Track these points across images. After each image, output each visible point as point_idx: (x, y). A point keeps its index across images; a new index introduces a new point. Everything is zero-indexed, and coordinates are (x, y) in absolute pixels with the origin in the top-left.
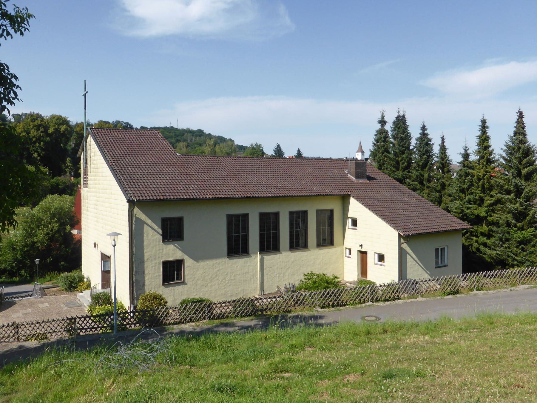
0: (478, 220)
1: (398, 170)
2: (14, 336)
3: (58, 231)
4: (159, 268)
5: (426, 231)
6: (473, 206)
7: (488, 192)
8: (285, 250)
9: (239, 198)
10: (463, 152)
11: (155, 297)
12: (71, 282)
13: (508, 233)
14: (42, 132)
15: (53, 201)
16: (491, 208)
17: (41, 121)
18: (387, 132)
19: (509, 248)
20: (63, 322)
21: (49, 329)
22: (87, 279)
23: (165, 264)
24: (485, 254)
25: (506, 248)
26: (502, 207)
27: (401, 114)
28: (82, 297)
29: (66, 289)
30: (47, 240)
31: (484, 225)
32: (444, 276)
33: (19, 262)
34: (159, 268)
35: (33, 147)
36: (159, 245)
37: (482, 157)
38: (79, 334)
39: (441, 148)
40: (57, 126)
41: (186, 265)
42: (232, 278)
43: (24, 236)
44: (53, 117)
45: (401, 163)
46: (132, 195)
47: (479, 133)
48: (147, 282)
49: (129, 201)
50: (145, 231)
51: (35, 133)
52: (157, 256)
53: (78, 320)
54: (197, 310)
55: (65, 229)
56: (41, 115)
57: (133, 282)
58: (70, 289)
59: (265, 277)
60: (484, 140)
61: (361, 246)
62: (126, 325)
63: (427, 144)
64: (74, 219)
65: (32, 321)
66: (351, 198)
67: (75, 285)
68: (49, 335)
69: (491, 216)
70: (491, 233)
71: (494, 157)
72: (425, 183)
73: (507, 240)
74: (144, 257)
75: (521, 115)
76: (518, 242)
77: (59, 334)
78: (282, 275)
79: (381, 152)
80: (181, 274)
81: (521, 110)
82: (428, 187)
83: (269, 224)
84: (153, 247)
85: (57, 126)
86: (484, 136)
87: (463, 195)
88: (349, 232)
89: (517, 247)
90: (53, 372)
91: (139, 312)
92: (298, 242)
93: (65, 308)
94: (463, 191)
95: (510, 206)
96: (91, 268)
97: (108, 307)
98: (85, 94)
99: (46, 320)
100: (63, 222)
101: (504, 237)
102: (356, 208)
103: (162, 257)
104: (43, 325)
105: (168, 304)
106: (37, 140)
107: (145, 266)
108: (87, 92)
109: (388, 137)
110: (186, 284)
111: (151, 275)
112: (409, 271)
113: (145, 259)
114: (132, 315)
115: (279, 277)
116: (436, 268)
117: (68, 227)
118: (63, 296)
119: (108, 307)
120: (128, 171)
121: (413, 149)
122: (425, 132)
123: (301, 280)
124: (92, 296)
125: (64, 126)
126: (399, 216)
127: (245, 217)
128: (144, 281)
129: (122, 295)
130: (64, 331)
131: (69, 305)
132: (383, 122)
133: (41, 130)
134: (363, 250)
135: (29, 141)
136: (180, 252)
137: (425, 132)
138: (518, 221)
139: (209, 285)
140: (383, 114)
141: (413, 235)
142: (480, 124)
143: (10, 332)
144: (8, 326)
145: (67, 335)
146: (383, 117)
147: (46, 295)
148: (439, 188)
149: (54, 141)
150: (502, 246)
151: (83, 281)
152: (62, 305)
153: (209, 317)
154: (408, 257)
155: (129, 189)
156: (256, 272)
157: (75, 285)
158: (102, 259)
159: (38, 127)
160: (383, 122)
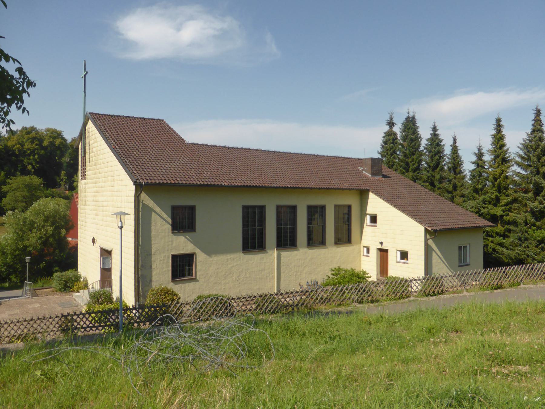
0: (494, 219)
1: (407, 171)
3: (53, 235)
5: (453, 227)
6: (490, 206)
7: (504, 191)
9: (256, 187)
10: (477, 152)
11: (167, 292)
12: (66, 282)
13: (527, 232)
14: (37, 145)
15: (47, 204)
16: (508, 207)
17: (36, 134)
18: (395, 134)
19: (528, 247)
20: (56, 320)
22: (84, 279)
23: (175, 258)
24: (502, 254)
25: (525, 247)
27: (411, 115)
28: (79, 296)
29: (60, 290)
30: (40, 244)
31: (499, 225)
33: (10, 267)
35: (28, 159)
37: (497, 157)
39: (452, 149)
42: (248, 275)
43: (16, 239)
44: (48, 130)
45: (413, 165)
46: (139, 178)
47: (494, 132)
48: (154, 278)
49: (135, 183)
51: (30, 146)
54: (218, 306)
55: (60, 233)
56: (36, 128)
58: (65, 290)
59: (282, 275)
60: (499, 139)
61: (381, 243)
63: (438, 145)
64: (67, 223)
65: (18, 318)
66: (371, 194)
69: (507, 215)
70: (507, 233)
71: (509, 156)
72: (436, 184)
73: (526, 239)
74: (151, 250)
75: (538, 113)
76: (538, 241)
77: (52, 334)
78: (299, 274)
79: (389, 153)
80: (192, 270)
81: (539, 108)
82: (439, 188)
83: (286, 216)
85: (51, 140)
86: (499, 134)
87: (477, 196)
89: (537, 246)
90: (38, 373)
91: (149, 308)
92: (316, 240)
94: (476, 191)
95: (530, 204)
96: (88, 267)
99: (35, 318)
101: (523, 236)
102: (375, 204)
103: (171, 250)
105: (181, 301)
106: (31, 152)
107: (153, 259)
108: (87, 73)
109: (397, 138)
110: (198, 281)
113: (153, 251)
115: (296, 275)
116: (459, 266)
117: (63, 231)
118: (57, 296)
120: (133, 155)
121: (423, 151)
122: (437, 133)
123: (328, 276)
125: (60, 140)
126: (421, 212)
127: (262, 209)
129: (125, 291)
130: (58, 331)
132: (391, 124)
133: (35, 143)
134: (384, 247)
135: (23, 153)
136: (192, 245)
137: (437, 133)
138: (537, 219)
140: (391, 116)
142: (495, 122)
145: (62, 335)
146: (391, 119)
147: (37, 295)
148: (451, 189)
149: (49, 154)
151: (80, 281)
152: (56, 306)
154: (434, 254)
155: (135, 172)
156: (273, 269)
157: (69, 286)
158: (101, 255)
159: (33, 140)
160: (391, 124)
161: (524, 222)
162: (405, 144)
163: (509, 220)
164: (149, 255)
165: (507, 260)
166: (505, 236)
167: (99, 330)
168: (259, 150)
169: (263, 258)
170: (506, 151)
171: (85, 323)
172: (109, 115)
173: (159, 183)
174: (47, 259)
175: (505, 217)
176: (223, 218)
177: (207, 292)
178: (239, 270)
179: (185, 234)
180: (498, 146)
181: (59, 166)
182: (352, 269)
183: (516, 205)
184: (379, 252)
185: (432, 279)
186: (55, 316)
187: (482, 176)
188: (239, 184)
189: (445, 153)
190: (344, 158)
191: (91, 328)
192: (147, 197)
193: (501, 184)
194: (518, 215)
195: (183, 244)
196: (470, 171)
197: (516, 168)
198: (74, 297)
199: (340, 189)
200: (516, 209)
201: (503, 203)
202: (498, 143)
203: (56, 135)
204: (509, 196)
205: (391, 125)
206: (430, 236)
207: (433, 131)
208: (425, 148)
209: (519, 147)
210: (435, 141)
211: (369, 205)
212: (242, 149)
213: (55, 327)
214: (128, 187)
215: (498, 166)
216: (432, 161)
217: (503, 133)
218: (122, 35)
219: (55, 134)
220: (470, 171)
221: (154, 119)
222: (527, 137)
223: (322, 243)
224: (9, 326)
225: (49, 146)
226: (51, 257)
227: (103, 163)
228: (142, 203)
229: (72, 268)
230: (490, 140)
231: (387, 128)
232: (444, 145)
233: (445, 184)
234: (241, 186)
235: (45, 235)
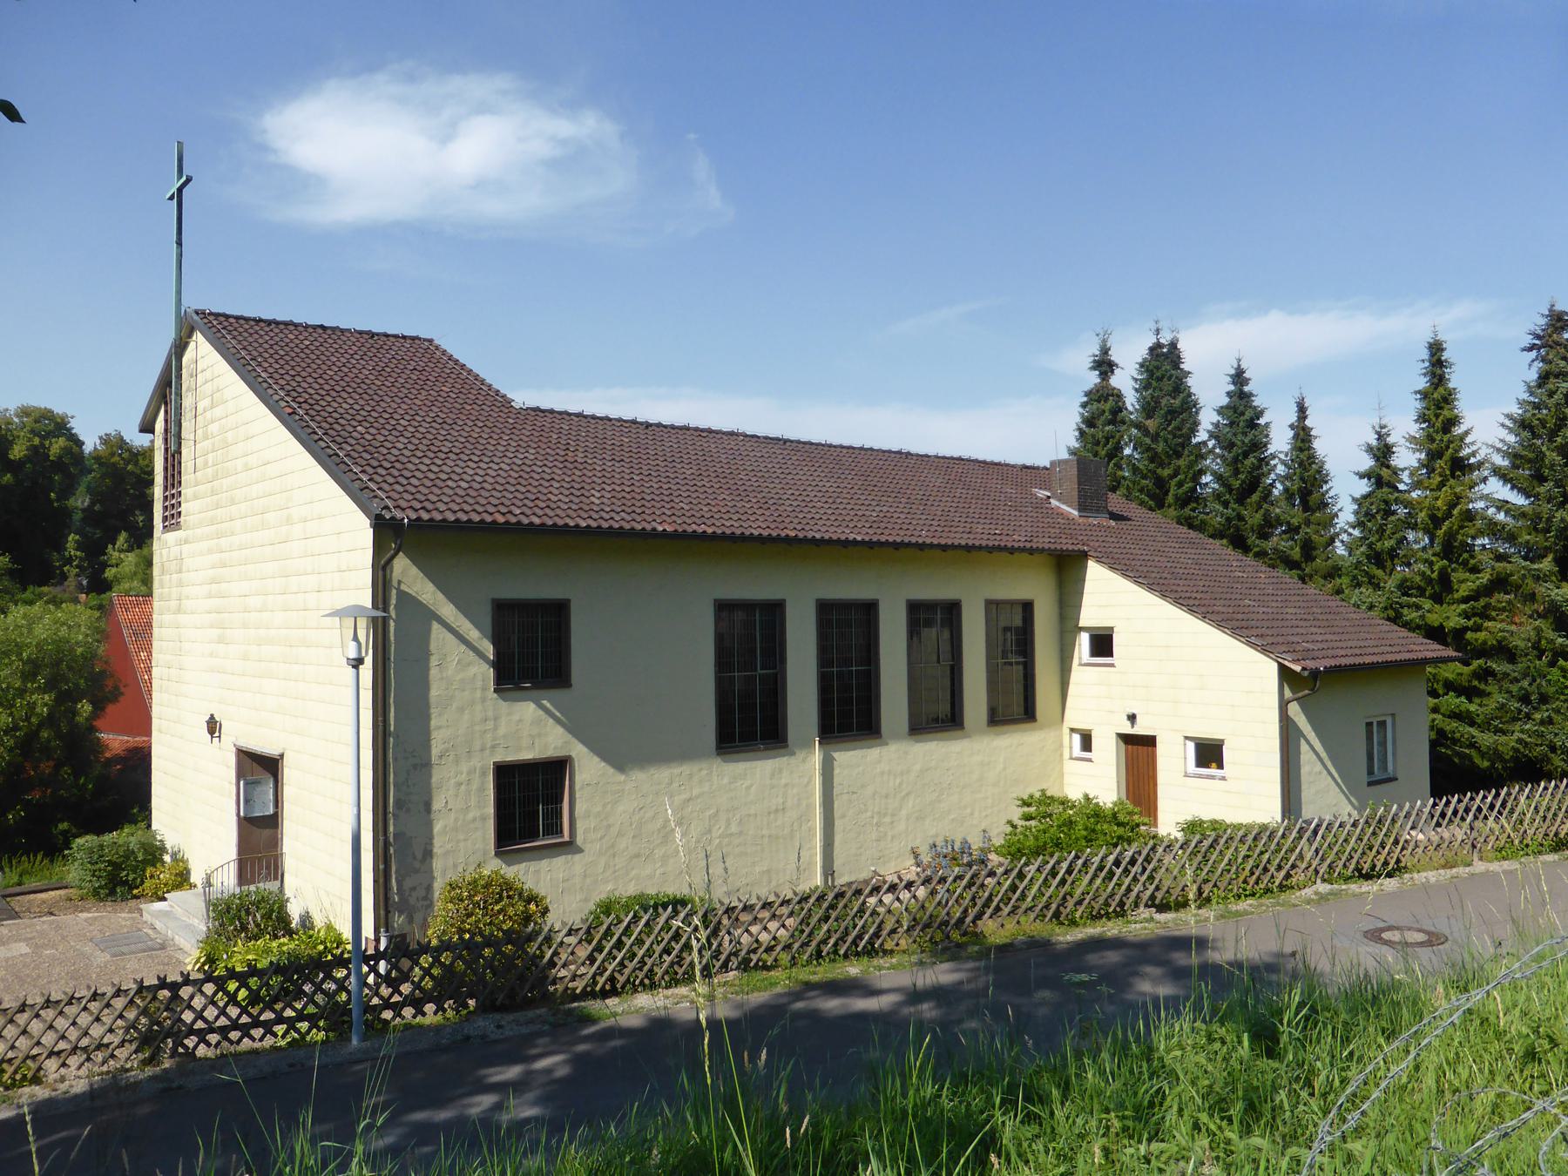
3: (50, 721)
4: (482, 789)
8: (897, 737)
9: (760, 539)
16: (1482, 602)
18: (1119, 396)
19: (1550, 721)
20: (119, 1003)
21: (49, 1039)
23: (507, 775)
25: (1542, 722)
26: (1510, 602)
29: (95, 893)
32: (1401, 808)
34: (482, 789)
37: (1433, 456)
38: (190, 1054)
39: (1296, 437)
40: (37, 441)
41: (579, 778)
42: (734, 829)
44: (25, 412)
45: (1180, 479)
46: (389, 503)
47: (1422, 383)
48: (438, 846)
50: (433, 646)
52: (477, 745)
53: (185, 992)
55: (75, 713)
57: (386, 844)
58: (112, 893)
60: (1438, 405)
61: (1132, 718)
67: (134, 875)
68: (51, 1065)
69: (1477, 628)
70: (1476, 683)
71: (1474, 454)
72: (1252, 539)
73: (1544, 699)
78: (887, 819)
80: (559, 814)
84: (461, 710)
85: (37, 441)
86: (1441, 389)
87: (1379, 573)
88: (1085, 675)
93: (102, 958)
94: (1377, 558)
96: (191, 813)
97: (287, 944)
99: (36, 999)
100: (68, 692)
102: (1106, 595)
103: (493, 747)
104: (22, 1019)
108: (189, 180)
110: (580, 851)
111: (453, 815)
112: (1307, 793)
113: (435, 752)
114: (382, 967)
116: (1370, 784)
117: (85, 708)
118: (85, 915)
119: (287, 944)
121: (1204, 443)
122: (1246, 389)
123: (1010, 823)
124: (208, 903)
125: (62, 442)
127: (774, 611)
128: (431, 838)
131: (115, 944)
132: (1104, 365)
134: (1139, 730)
136: (560, 730)
137: (1246, 389)
139: (658, 853)
140: (1104, 341)
141: (1328, 670)
142: (1425, 354)
146: (1105, 351)
148: (1296, 553)
150: (1528, 717)
152: (88, 949)
154: (1304, 747)
156: (810, 807)
158: (241, 773)
160: (1104, 365)
161: (1534, 647)
162: (1151, 424)
163: (1485, 642)
164: (422, 765)
165: (1486, 764)
166: (1470, 693)
168: (737, 434)
169: (781, 771)
170: (1462, 438)
171: (223, 1012)
172: (259, 321)
173: (457, 520)
174: (35, 796)
175: (1469, 635)
176: (656, 639)
177: (610, 887)
178: (708, 813)
179: (535, 693)
180: (1438, 425)
181: (62, 517)
182: (1087, 798)
183: (1501, 598)
184: (1122, 745)
185: (1380, 821)
186: (110, 991)
187: (1394, 513)
188: (710, 531)
189: (1271, 449)
190: (984, 462)
191: (245, 1031)
192: (414, 570)
193: (1452, 531)
194: (1513, 628)
196: (1354, 500)
197: (1497, 488)
198: (146, 917)
199: (1005, 549)
200: (1504, 609)
201: (1464, 591)
202: (1437, 416)
203: (52, 427)
204: (1479, 572)
205: (1104, 368)
206: (1293, 691)
207: (1234, 383)
208: (1212, 435)
209: (1503, 425)
210: (1243, 414)
212: (687, 428)
213: (111, 1031)
214: (355, 532)
215: (1442, 484)
216: (1236, 472)
217: (1451, 385)
219: (47, 425)
220: (1354, 500)
221: (404, 337)
222: (1525, 396)
225: (27, 459)
226: (43, 787)
227: (247, 469)
228: (398, 589)
229: (133, 821)
230: (1414, 405)
232: (1267, 425)
233: (1277, 541)
234: (714, 536)
235: (28, 719)
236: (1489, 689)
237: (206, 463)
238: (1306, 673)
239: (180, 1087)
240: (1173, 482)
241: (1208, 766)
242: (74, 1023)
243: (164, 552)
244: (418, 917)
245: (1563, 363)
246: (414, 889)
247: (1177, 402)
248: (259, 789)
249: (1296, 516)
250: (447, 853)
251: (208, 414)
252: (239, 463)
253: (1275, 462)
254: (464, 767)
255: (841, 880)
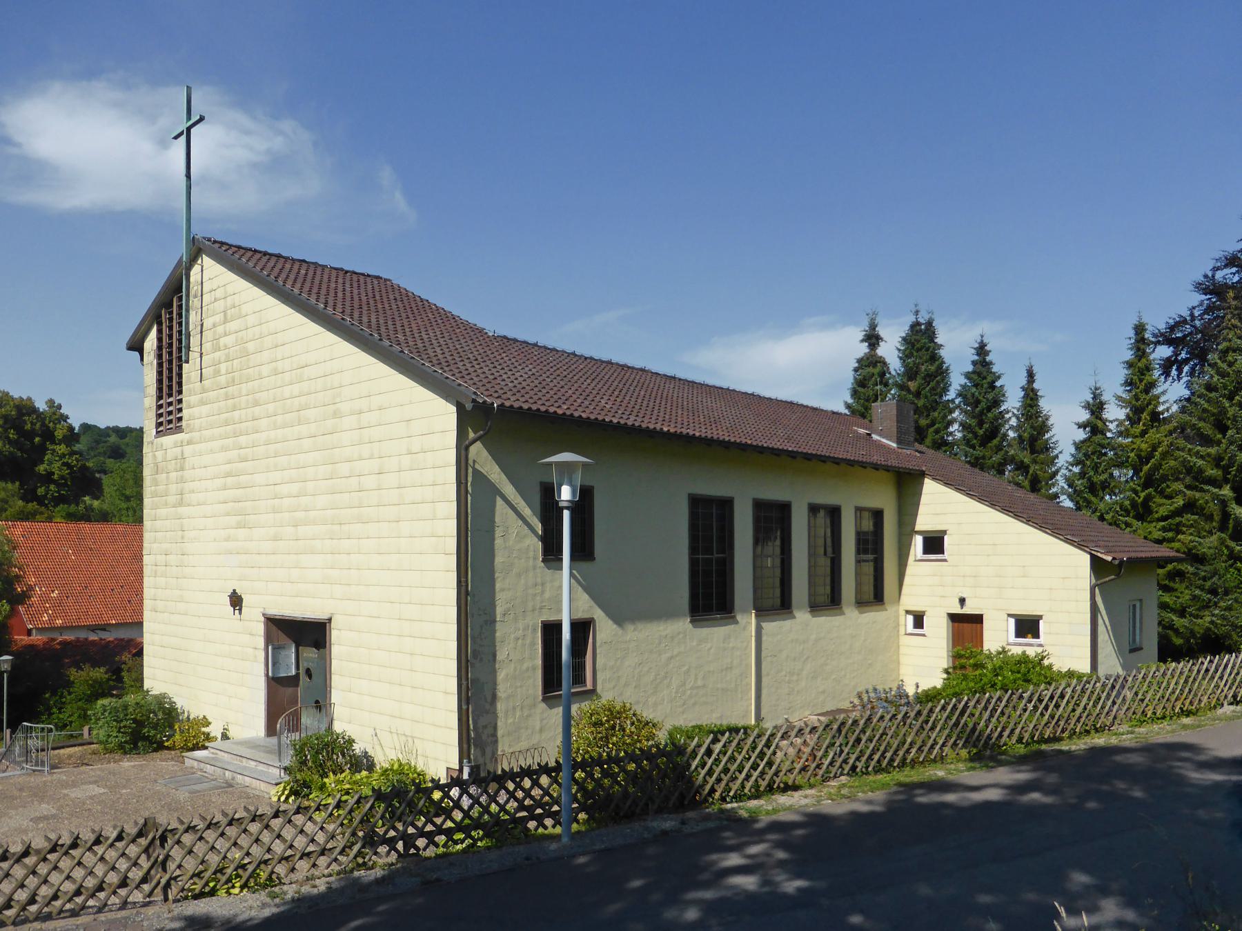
2: (144, 880)
4: (533, 644)
10: (1089, 397)
12: (139, 723)
26: (1195, 521)
29: (121, 746)
36: (535, 568)
39: (1026, 396)
42: (700, 683)
47: (1129, 355)
48: (503, 690)
50: (497, 519)
58: (136, 747)
61: (962, 601)
62: (524, 820)
63: (992, 386)
66: (926, 480)
78: (795, 678)
84: (519, 575)
86: (1144, 360)
87: (1093, 499)
98: (189, 129)
102: (939, 505)
107: (498, 634)
111: (513, 665)
121: (953, 401)
122: (988, 359)
127: (726, 505)
128: (495, 684)
132: (873, 339)
134: (967, 610)
139: (651, 700)
142: (1132, 333)
143: (131, 860)
144: (120, 838)
146: (873, 326)
150: (1216, 604)
153: (854, 768)
156: (749, 666)
158: (269, 640)
160: (873, 339)
167: (437, 846)
176: (651, 520)
183: (1189, 518)
192: (485, 453)
195: (565, 596)
198: (188, 763)
200: (1192, 526)
201: (1163, 511)
202: (1141, 381)
205: (874, 340)
208: (959, 395)
211: (922, 509)
216: (980, 424)
218: (19, 145)
223: (784, 606)
224: (201, 838)
228: (473, 468)
230: (1122, 373)
231: (863, 349)
236: (1176, 586)
237: (217, 373)
238: (1117, 562)
239: (438, 880)
240: (931, 430)
241: (1024, 637)
242: (322, 828)
243: (159, 454)
244: (488, 750)
245: (1239, 341)
246: (485, 727)
247: (933, 368)
248: (283, 653)
249: (1026, 457)
250: (508, 697)
251: (220, 329)
252: (265, 370)
253: (1007, 416)
254: (521, 625)
255: (768, 725)
